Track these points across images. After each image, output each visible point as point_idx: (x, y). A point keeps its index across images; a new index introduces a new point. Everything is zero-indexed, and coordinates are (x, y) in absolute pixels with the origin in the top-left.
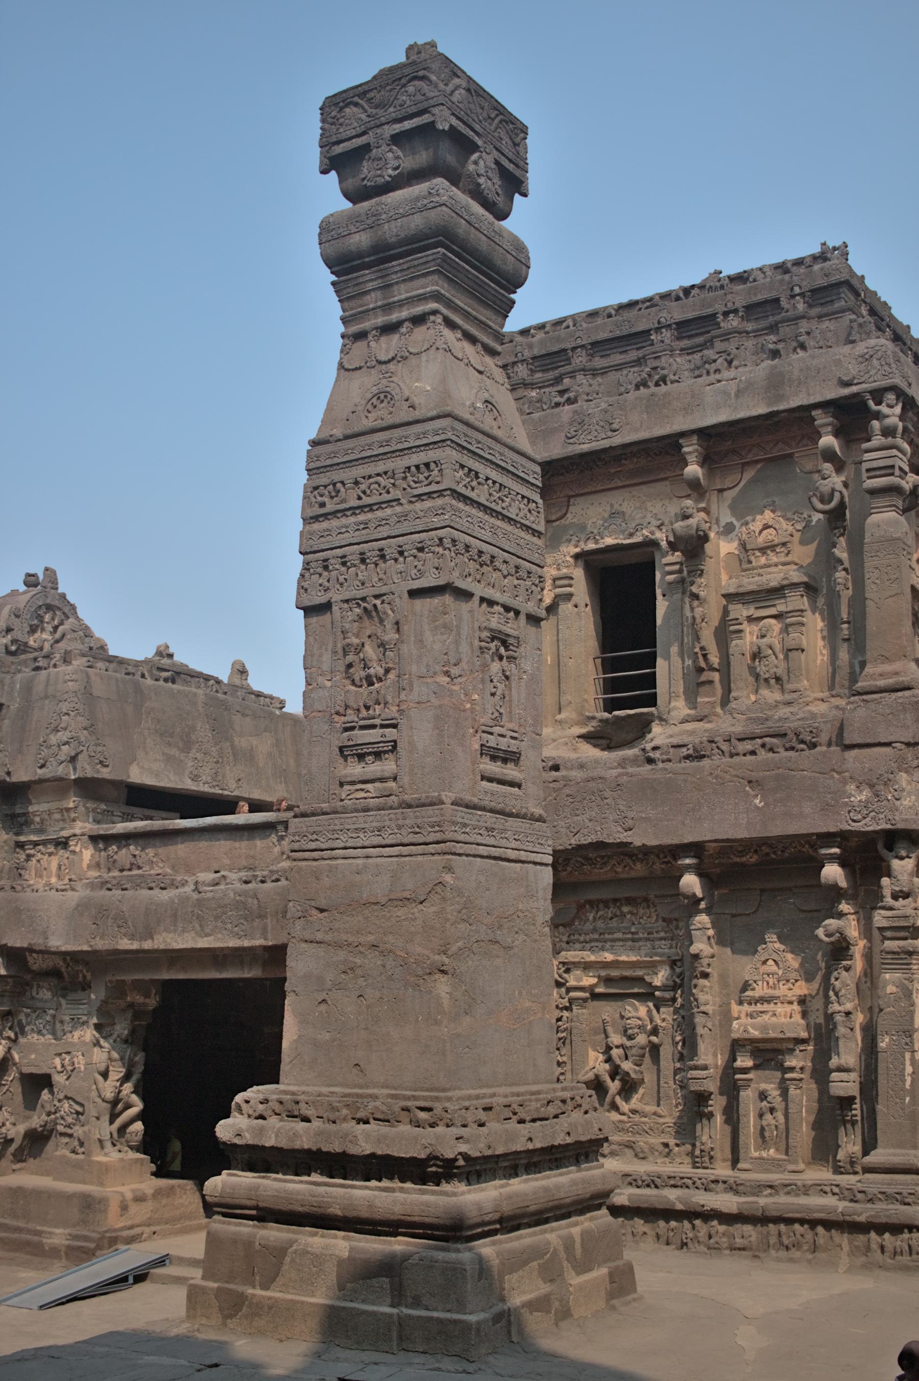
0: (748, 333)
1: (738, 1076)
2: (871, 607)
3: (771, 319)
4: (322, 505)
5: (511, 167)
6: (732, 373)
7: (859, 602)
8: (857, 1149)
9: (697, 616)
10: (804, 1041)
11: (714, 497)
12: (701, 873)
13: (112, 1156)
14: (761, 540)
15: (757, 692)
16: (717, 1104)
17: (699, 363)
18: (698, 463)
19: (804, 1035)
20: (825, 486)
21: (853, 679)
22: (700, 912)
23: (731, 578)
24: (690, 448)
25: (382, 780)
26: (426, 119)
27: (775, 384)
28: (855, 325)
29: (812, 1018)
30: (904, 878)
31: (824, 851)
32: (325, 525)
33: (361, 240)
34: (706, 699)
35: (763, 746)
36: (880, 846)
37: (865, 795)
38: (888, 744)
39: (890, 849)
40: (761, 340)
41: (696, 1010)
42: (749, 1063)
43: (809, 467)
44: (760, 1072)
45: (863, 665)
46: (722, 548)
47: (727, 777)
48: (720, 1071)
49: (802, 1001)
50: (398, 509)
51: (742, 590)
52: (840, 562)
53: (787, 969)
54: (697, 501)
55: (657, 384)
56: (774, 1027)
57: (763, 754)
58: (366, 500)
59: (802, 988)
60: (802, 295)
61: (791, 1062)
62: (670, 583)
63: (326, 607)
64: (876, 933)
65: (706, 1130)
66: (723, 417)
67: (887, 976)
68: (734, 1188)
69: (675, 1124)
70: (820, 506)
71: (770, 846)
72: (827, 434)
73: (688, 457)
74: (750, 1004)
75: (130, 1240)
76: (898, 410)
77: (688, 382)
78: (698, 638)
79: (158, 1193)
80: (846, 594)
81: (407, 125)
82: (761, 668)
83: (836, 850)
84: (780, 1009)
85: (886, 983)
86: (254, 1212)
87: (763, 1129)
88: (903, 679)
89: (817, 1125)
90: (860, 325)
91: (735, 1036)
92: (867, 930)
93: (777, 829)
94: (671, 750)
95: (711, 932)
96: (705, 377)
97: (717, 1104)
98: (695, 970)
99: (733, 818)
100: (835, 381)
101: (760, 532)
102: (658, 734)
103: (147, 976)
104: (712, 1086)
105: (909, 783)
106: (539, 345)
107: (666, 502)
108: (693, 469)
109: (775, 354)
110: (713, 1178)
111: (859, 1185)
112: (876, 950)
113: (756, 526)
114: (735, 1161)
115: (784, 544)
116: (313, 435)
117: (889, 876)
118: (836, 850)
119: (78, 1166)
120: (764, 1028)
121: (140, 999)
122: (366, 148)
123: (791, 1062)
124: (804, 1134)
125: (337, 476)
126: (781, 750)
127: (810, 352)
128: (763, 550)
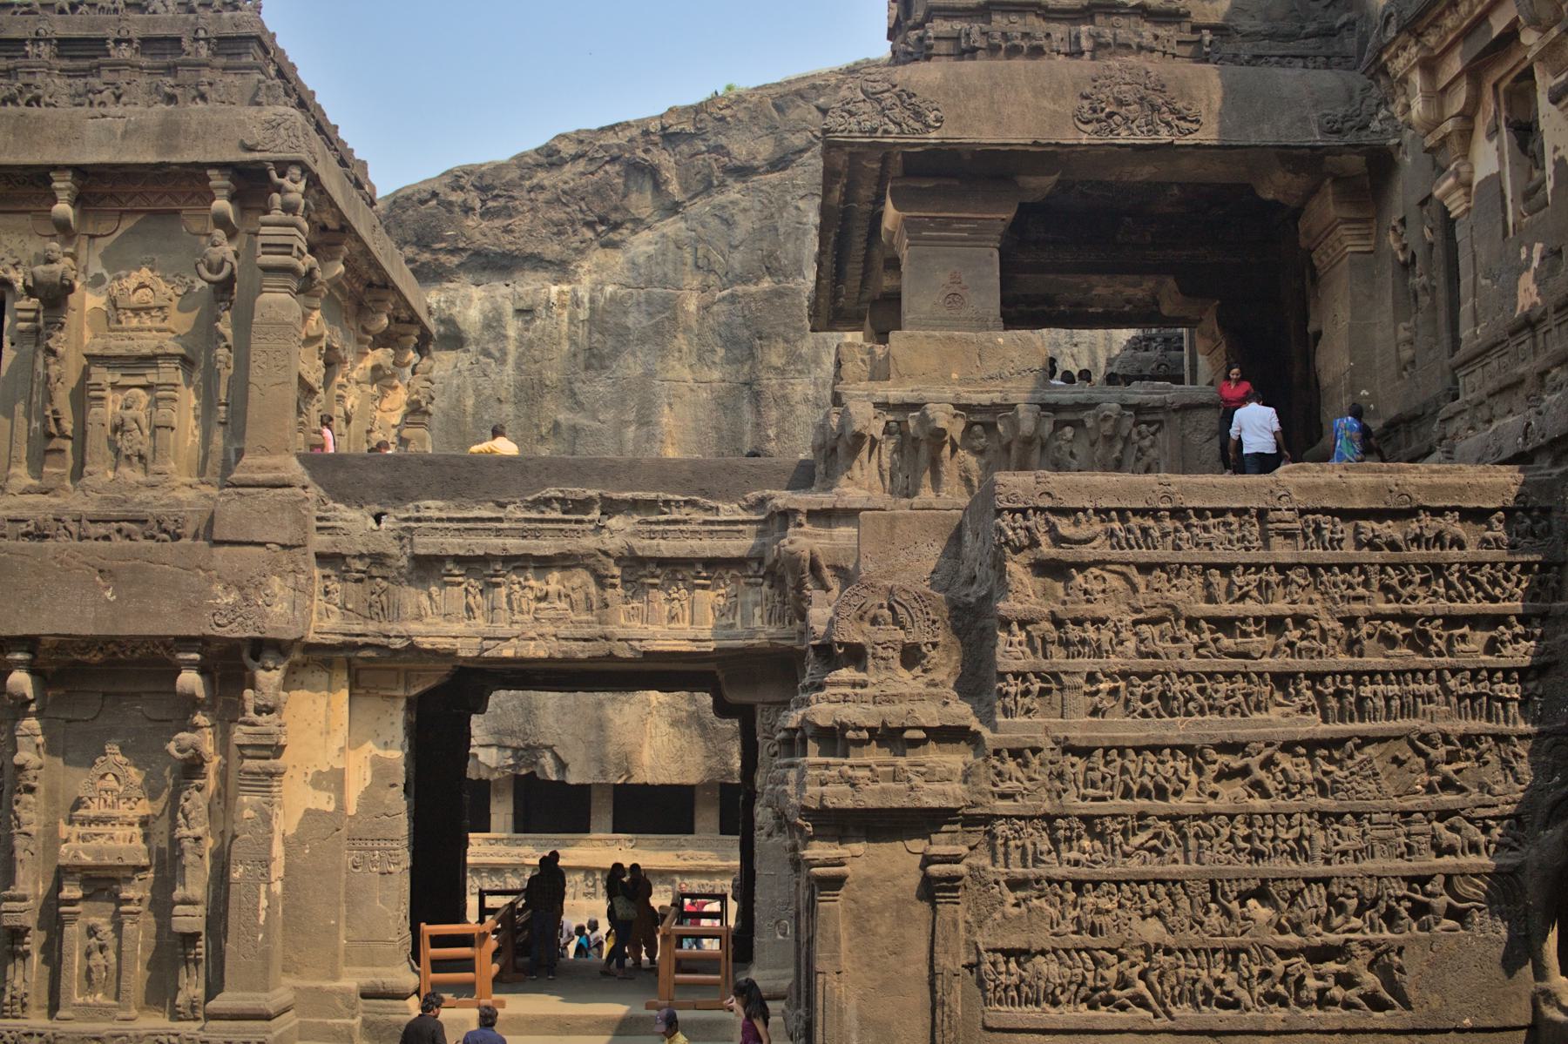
0: (141, 68)
1: (63, 909)
2: (254, 393)
3: (169, 59)
7: (241, 383)
8: (200, 992)
9: (52, 374)
10: (144, 869)
11: (84, 243)
12: (33, 671)
14: (135, 299)
15: (115, 469)
16: (34, 942)
17: (81, 90)
18: (69, 202)
19: (145, 861)
20: (215, 254)
21: (227, 468)
22: (30, 715)
23: (96, 337)
24: (63, 185)
28: (263, 86)
29: (155, 841)
30: (270, 691)
31: (181, 656)
34: (55, 470)
35: (119, 531)
36: (245, 655)
37: (232, 597)
38: (262, 544)
39: (256, 657)
40: (157, 79)
41: (16, 830)
42: (78, 894)
43: (197, 228)
44: (90, 904)
45: (240, 453)
46: (89, 301)
47: (75, 563)
48: (40, 901)
49: (144, 822)
51: (107, 353)
52: (224, 338)
53: (128, 786)
54: (63, 244)
55: (28, 104)
56: (110, 853)
57: (118, 542)
59: (144, 808)
60: (207, 40)
61: (128, 892)
62: (22, 332)
64: (234, 750)
65: (20, 972)
66: (105, 157)
67: (245, 799)
70: (207, 275)
71: (119, 645)
72: (222, 197)
73: (58, 194)
74: (82, 824)
76: (302, 186)
77: (65, 110)
78: (50, 399)
80: (225, 374)
82: (123, 443)
83: (196, 656)
84: (119, 831)
85: (243, 806)
87: (89, 970)
88: (285, 475)
89: (154, 964)
90: (268, 87)
91: (62, 862)
92: (223, 745)
93: (130, 627)
94: (8, 525)
95: (40, 739)
96: (86, 107)
97: (34, 942)
98: (18, 782)
100: (236, 143)
101: (135, 290)
104: (30, 920)
105: (282, 588)
107: (26, 239)
108: (63, 208)
109: (171, 99)
110: (25, 1030)
111: (202, 1034)
112: (233, 768)
113: (132, 283)
114: (53, 1008)
115: (161, 308)
117: (253, 687)
118: (196, 656)
120: (98, 853)
123: (128, 892)
124: (137, 975)
126: (140, 538)
127: (211, 105)
128: (136, 311)
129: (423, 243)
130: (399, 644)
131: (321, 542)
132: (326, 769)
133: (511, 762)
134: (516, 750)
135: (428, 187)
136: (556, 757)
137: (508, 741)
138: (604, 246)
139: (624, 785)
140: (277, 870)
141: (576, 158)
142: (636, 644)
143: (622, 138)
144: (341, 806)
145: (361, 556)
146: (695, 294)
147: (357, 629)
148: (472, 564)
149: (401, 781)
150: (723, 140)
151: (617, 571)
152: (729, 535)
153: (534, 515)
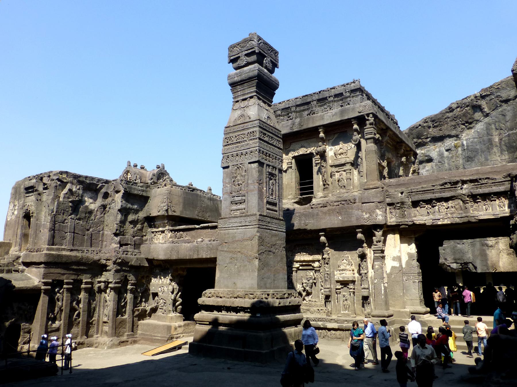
4: (228, 142)
5: (274, 61)
6: (331, 111)
13: (172, 314)
14: (339, 152)
25: (242, 209)
26: (253, 50)
27: (342, 113)
32: (228, 147)
33: (236, 79)
50: (246, 143)
56: (346, 277)
57: (341, 205)
58: (238, 141)
63: (227, 167)
68: (336, 321)
69: (256, 92)
75: (177, 338)
79: (185, 325)
81: (250, 51)
84: (347, 272)
86: (208, 323)
99: (335, 221)
102: (314, 201)
103: (184, 267)
106: (282, 106)
116: (226, 126)
119: (164, 317)
120: (343, 277)
121: (182, 272)
122: (239, 57)
125: (231, 135)
128: (340, 154)
129: (418, 137)
130: (410, 223)
131: (388, 200)
132: (396, 256)
133: (461, 267)
134: (461, 264)
135: (418, 124)
136: (473, 265)
137: (458, 261)
138: (468, 129)
139: (495, 272)
140: (386, 280)
141: (457, 108)
142: (476, 218)
143: (469, 100)
144: (401, 266)
145: (398, 203)
146: (497, 137)
147: (400, 221)
148: (429, 202)
149: (416, 258)
150: (499, 94)
151: (468, 199)
152: (500, 185)
153: (443, 187)
